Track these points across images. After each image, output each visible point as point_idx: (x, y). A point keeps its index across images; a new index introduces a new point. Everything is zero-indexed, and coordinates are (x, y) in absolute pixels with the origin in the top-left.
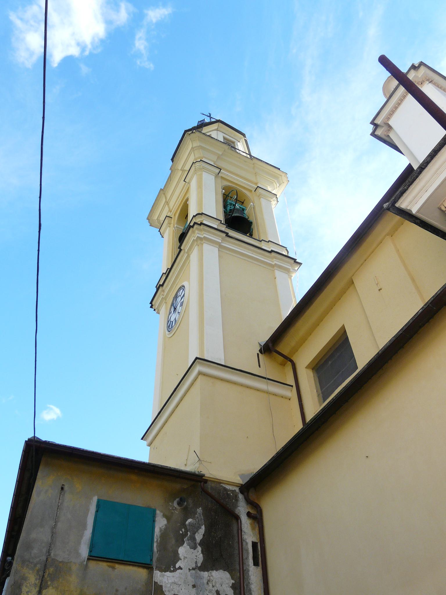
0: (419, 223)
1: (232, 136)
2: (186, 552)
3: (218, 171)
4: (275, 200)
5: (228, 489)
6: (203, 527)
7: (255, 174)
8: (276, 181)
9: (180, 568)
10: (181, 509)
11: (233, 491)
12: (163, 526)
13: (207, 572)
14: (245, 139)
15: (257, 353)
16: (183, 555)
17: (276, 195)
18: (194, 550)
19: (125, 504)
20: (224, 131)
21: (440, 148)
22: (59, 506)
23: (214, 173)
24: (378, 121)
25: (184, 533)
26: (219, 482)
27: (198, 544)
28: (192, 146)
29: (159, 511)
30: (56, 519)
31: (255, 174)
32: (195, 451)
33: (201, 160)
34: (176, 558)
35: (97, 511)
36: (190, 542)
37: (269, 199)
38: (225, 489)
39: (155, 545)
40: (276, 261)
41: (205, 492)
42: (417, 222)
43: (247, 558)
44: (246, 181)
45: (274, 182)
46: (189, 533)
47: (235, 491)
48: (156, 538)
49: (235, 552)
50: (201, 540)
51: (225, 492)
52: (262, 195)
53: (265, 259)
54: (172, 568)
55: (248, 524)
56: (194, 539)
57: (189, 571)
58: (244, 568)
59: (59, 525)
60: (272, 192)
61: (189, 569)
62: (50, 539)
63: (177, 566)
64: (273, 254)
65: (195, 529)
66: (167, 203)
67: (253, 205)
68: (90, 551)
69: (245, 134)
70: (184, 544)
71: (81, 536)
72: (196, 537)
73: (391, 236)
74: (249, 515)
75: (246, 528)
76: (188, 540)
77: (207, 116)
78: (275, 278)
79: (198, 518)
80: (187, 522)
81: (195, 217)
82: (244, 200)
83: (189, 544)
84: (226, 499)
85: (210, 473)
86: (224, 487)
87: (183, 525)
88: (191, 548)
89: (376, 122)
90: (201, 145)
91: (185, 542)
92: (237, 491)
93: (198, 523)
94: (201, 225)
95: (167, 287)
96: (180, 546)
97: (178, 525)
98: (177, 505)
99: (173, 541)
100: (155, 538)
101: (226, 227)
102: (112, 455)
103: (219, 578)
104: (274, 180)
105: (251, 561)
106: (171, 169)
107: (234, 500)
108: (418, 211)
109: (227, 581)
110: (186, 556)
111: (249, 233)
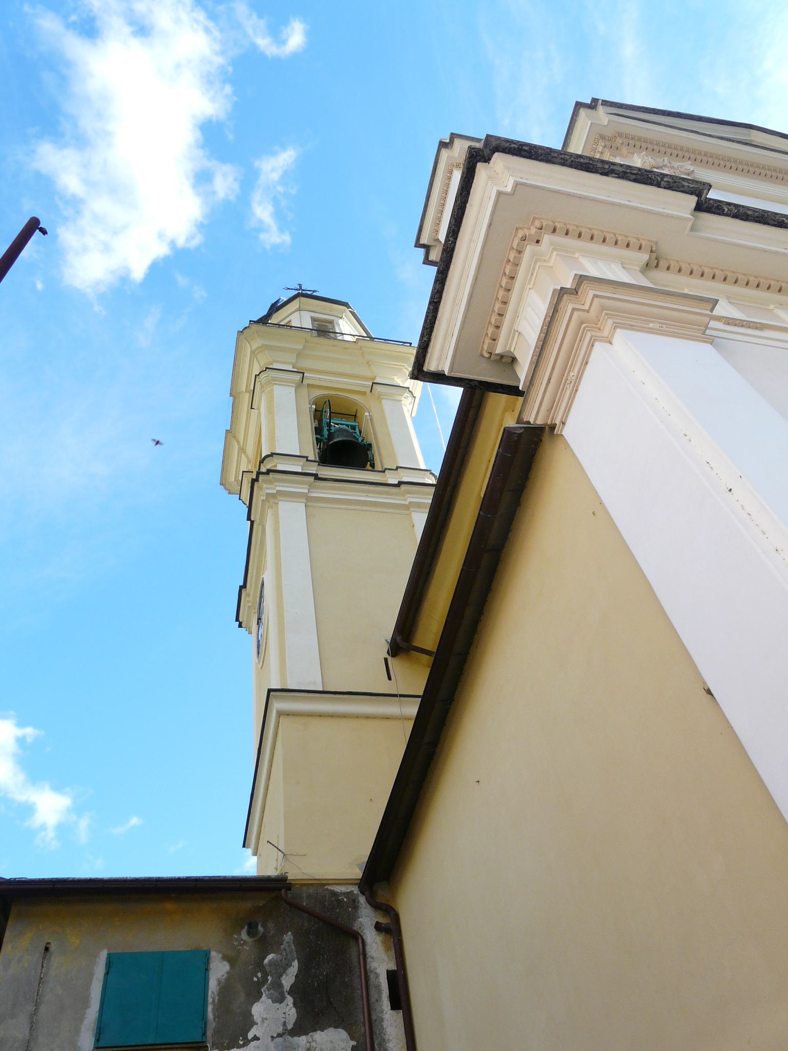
0: (477, 385)
1: (324, 311)
2: (265, 1010)
3: (299, 376)
4: (408, 397)
5: (338, 892)
6: (296, 964)
7: (368, 363)
8: (406, 365)
9: (256, 1038)
10: (253, 941)
11: (348, 893)
12: (223, 976)
13: (304, 1036)
14: (350, 311)
15: (385, 658)
16: (260, 1016)
17: (408, 388)
18: (280, 1004)
19: (153, 953)
20: (312, 309)
21: (446, 266)
22: (42, 979)
23: (291, 382)
24: (424, 240)
25: (261, 980)
26: (320, 884)
27: (286, 994)
28: (251, 349)
29: (216, 951)
30: (37, 1000)
31: (368, 363)
32: (268, 842)
33: (267, 368)
34: (249, 1022)
35: (107, 973)
36: (273, 992)
37: (398, 398)
38: (334, 894)
39: (210, 1008)
40: (410, 497)
41: (296, 907)
42: (473, 385)
43: (379, 1000)
44: (354, 380)
45: (403, 367)
46: (270, 978)
47: (351, 892)
48: (211, 997)
49: (355, 995)
50: (291, 985)
51: (333, 899)
52: (383, 395)
53: (391, 499)
54: (241, 1041)
55: (378, 942)
56: (280, 986)
57: (272, 1040)
58: (374, 1017)
59: (43, 1009)
60: (404, 386)
61: (272, 1037)
62: (27, 1034)
63: (250, 1035)
64: (403, 487)
65: (281, 968)
66: (242, 450)
67: (370, 415)
68: (97, 1040)
69: (348, 303)
70: (261, 997)
71: (81, 1019)
72: (284, 982)
73: (512, 410)
74: (378, 927)
75: (375, 951)
76: (269, 989)
77: (295, 289)
78: (413, 526)
79: (285, 950)
80: (266, 961)
81: (263, 463)
82: (356, 411)
83: (269, 997)
84: (336, 909)
85: (303, 873)
86: (331, 891)
87: (259, 965)
88: (274, 1001)
89: (423, 241)
90: (263, 343)
91: (264, 994)
92: (355, 892)
93: (285, 959)
94: (269, 474)
95: (251, 586)
96: (255, 1003)
97: (250, 968)
98: (247, 937)
99: (242, 997)
100: (209, 997)
101: (318, 465)
102: (123, 878)
103: (327, 1041)
104: (403, 364)
105: (386, 1003)
106: (231, 395)
107: (350, 907)
108: (451, 369)
109: (342, 1045)
110: (265, 1017)
111: (369, 463)
